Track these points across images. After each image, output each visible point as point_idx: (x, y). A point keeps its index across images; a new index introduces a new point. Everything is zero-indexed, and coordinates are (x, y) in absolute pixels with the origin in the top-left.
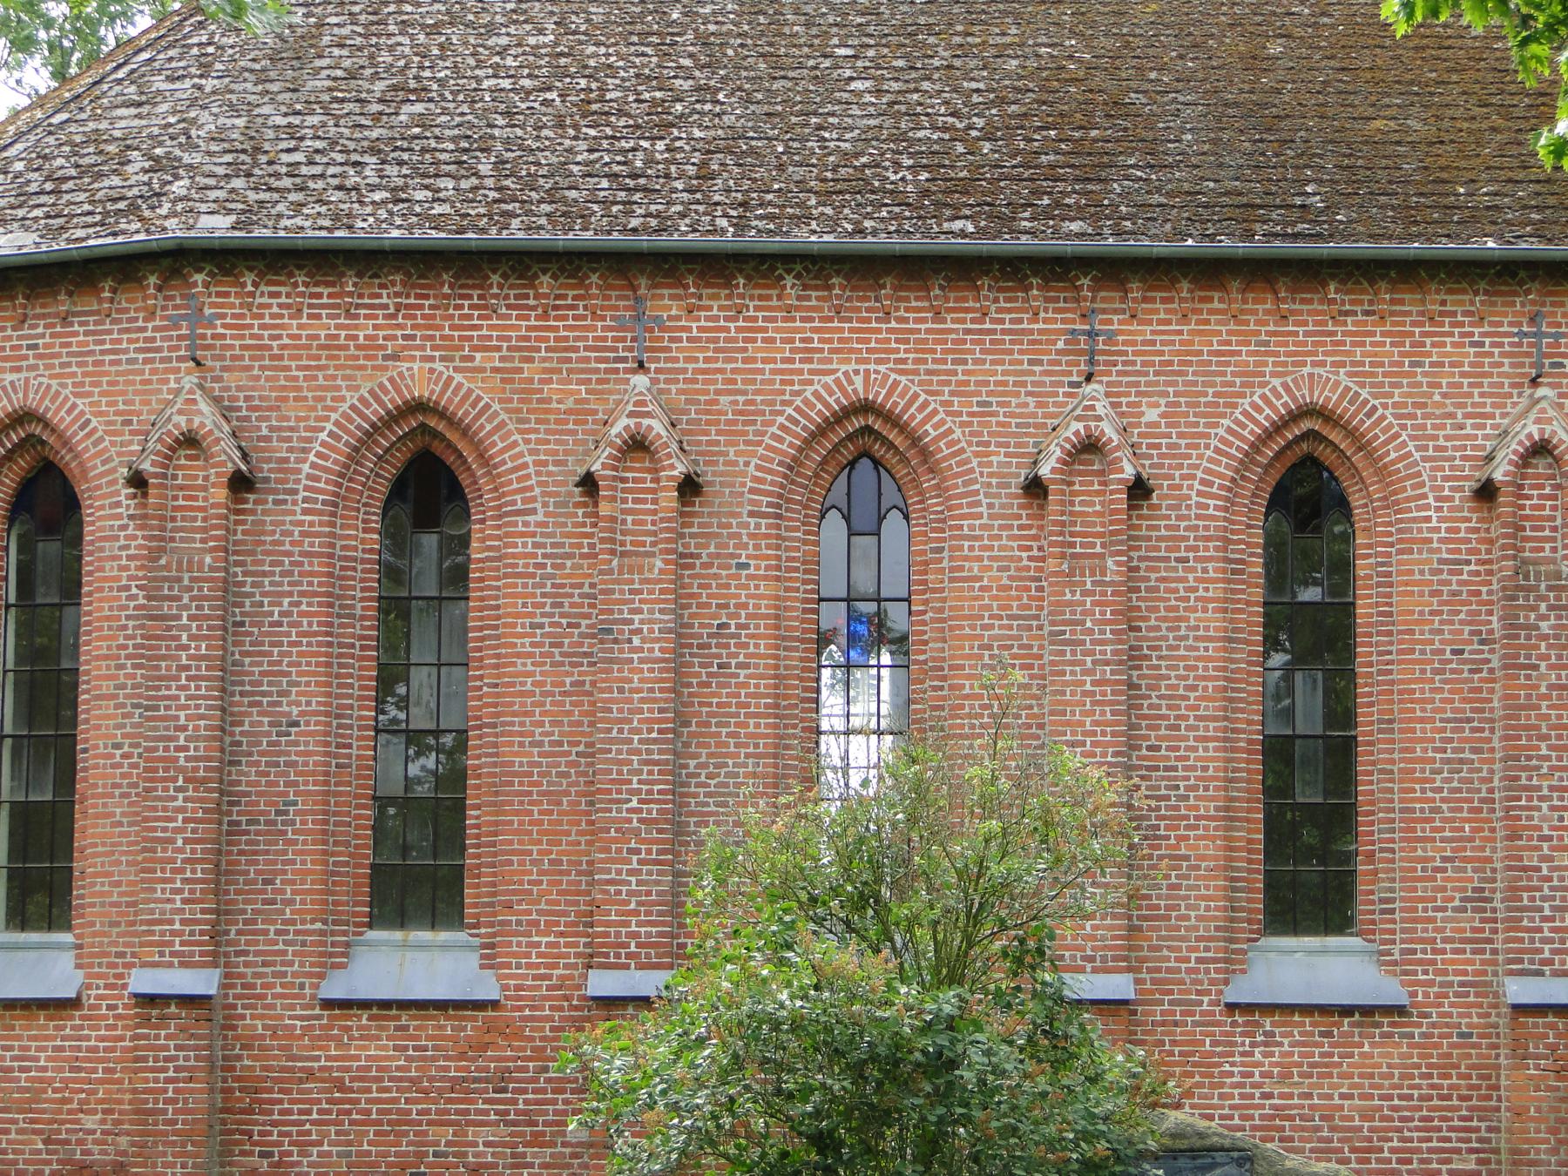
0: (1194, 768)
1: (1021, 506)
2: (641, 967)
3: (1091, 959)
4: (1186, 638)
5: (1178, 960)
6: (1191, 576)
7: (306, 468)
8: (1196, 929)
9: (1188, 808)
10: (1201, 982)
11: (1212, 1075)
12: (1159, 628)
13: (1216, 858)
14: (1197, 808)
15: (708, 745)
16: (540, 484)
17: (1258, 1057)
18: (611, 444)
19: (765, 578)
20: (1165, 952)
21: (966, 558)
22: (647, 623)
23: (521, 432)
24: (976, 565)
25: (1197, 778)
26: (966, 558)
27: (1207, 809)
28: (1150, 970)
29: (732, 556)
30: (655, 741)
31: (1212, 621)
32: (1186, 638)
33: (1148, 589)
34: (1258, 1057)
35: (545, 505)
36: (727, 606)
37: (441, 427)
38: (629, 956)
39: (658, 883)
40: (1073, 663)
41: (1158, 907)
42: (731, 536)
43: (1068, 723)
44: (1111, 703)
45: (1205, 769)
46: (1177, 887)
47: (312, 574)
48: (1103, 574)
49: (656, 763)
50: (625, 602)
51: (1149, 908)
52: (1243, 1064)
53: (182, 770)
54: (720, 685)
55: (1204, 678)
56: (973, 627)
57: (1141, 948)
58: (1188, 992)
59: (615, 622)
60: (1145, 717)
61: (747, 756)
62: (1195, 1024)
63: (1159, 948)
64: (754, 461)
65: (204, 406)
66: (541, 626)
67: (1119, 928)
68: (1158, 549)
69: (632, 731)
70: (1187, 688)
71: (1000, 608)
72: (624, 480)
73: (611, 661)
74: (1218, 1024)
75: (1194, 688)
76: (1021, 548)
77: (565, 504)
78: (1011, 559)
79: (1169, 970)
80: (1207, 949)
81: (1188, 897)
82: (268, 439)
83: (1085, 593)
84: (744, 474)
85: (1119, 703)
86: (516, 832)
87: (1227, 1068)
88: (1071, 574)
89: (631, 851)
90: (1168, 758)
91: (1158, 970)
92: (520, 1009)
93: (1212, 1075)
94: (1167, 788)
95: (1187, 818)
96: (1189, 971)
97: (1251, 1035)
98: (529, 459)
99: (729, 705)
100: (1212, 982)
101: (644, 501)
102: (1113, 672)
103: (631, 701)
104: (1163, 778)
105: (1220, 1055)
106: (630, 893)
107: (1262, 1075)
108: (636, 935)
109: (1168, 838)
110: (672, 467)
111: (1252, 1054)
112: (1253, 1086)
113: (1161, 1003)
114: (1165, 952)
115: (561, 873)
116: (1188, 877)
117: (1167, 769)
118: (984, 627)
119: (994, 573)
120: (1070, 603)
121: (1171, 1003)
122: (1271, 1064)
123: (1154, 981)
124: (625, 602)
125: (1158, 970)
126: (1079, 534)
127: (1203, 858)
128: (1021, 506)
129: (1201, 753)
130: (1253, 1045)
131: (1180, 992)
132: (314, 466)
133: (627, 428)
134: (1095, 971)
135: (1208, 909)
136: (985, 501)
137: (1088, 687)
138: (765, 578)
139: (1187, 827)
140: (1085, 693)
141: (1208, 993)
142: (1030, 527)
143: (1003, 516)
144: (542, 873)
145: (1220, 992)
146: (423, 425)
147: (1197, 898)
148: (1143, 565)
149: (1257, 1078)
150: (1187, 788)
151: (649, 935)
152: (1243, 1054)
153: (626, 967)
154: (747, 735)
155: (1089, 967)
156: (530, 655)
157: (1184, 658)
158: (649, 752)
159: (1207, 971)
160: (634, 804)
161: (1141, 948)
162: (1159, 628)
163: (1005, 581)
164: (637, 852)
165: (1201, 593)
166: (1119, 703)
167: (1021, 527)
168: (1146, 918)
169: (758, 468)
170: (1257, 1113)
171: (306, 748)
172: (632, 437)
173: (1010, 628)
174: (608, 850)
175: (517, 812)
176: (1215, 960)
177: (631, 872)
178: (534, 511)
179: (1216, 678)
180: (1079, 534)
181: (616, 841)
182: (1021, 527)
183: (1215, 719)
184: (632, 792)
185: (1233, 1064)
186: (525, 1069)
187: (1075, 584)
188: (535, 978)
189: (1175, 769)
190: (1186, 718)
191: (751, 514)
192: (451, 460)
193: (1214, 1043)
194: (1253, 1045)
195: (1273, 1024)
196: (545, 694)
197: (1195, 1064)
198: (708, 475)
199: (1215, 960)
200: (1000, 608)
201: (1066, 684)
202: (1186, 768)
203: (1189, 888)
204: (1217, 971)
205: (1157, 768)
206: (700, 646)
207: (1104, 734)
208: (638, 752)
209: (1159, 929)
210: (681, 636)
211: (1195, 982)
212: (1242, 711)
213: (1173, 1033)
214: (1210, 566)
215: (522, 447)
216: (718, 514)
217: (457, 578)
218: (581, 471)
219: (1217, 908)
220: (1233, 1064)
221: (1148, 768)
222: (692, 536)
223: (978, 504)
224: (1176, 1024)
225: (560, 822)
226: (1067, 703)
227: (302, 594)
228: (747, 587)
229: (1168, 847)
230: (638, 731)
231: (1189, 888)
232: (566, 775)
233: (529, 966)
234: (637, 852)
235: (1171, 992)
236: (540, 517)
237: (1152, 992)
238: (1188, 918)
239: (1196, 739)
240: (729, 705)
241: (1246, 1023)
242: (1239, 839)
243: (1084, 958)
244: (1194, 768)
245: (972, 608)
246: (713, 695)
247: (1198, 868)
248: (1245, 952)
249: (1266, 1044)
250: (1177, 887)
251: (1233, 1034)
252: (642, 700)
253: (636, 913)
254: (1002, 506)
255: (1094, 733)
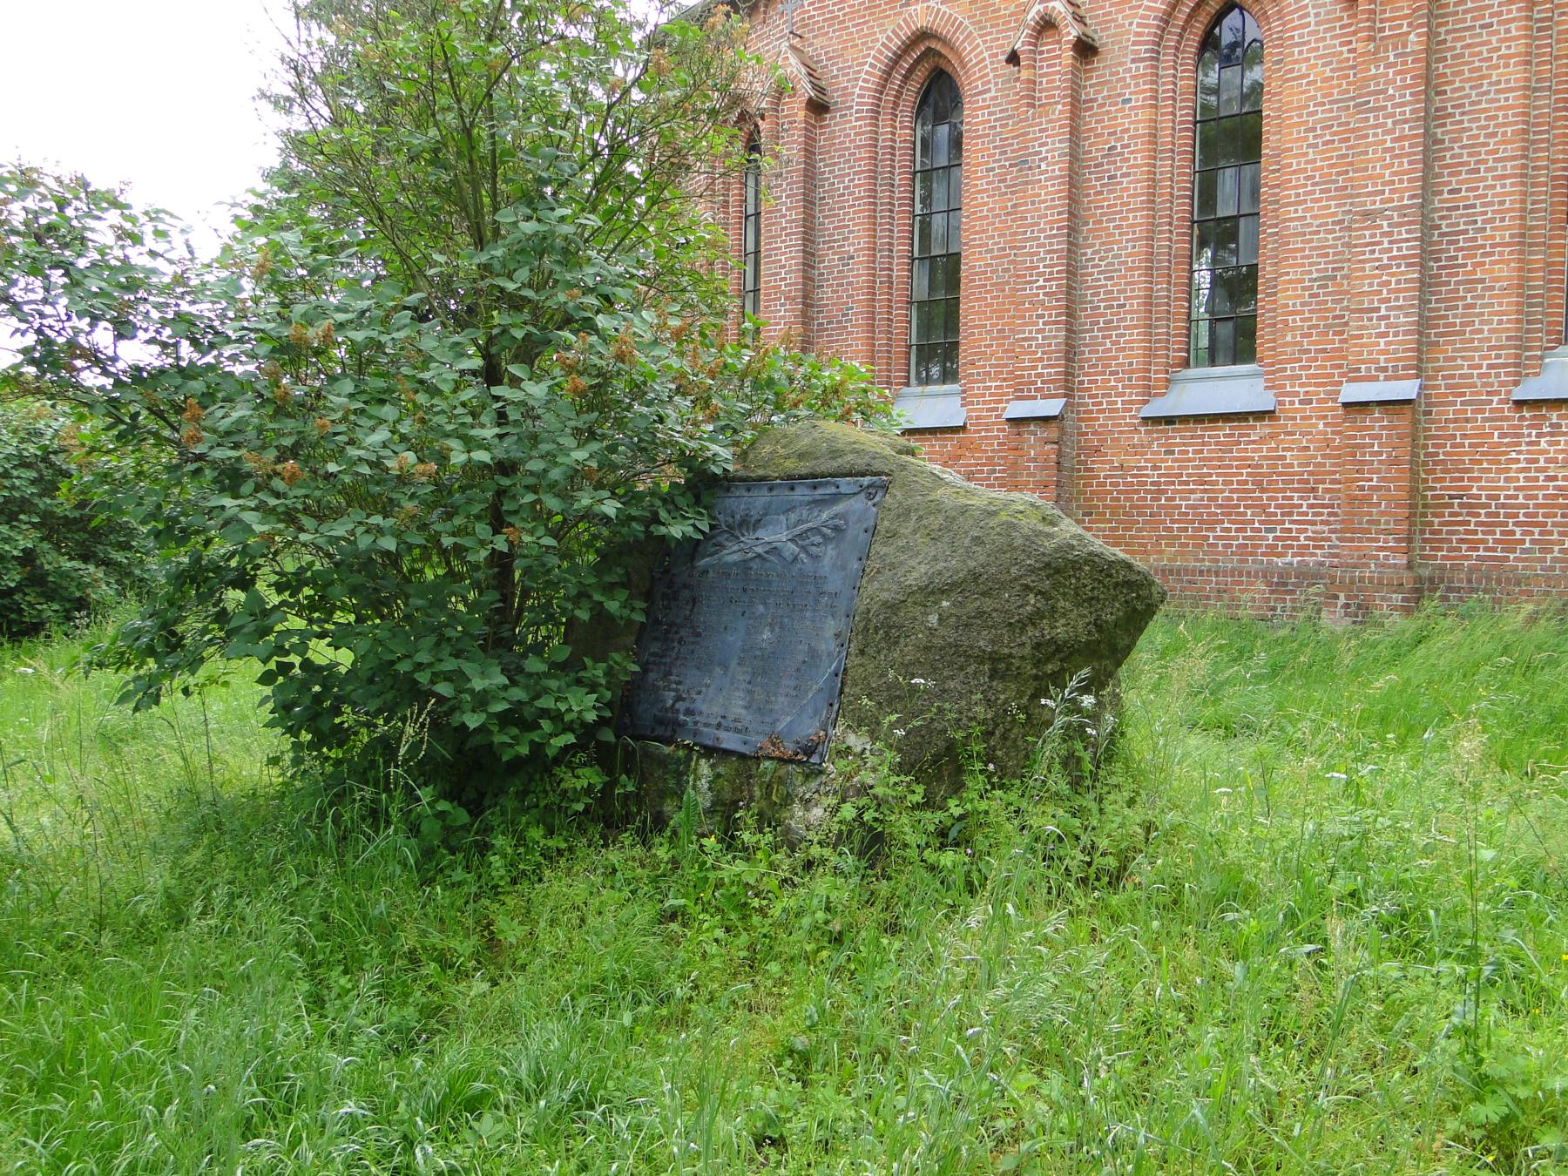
0: (1491, 204)
1: (1343, 10)
2: (1044, 397)
3: (1385, 369)
4: (1488, 92)
5: (1470, 367)
6: (1494, 39)
7: (857, 91)
8: (1489, 340)
9: (1485, 238)
10: (1492, 385)
11: (1499, 462)
12: (1463, 89)
13: (1509, 278)
14: (1493, 237)
15: (1100, 237)
16: (993, 70)
17: (1544, 445)
18: (1028, 26)
19: (1142, 107)
20: (1459, 362)
21: (1296, 62)
22: (1052, 150)
23: (981, 36)
24: (1304, 66)
25: (1494, 212)
26: (1296, 62)
27: (1503, 237)
28: (1444, 377)
29: (1120, 95)
30: (1055, 236)
31: (1514, 74)
32: (1488, 92)
33: (1454, 57)
34: (1544, 445)
35: (996, 84)
36: (1115, 133)
37: (938, 47)
38: (1037, 390)
39: (1055, 337)
40: (1376, 126)
41: (1454, 325)
42: (1118, 81)
43: (1370, 177)
44: (1409, 154)
45: (1502, 203)
46: (1473, 306)
47: (861, 159)
48: (1405, 46)
49: (1056, 251)
50: (1036, 139)
51: (1446, 325)
52: (1528, 452)
53: (783, 293)
54: (1110, 192)
55: (1505, 125)
56: (1300, 116)
57: (1438, 360)
58: (1479, 393)
59: (1030, 154)
60: (1447, 166)
61: (1128, 241)
62: (1485, 420)
63: (1454, 359)
64: (1137, 20)
65: (793, 60)
66: (993, 169)
67: (1410, 342)
68: (1464, 21)
69: (1040, 231)
70: (1488, 136)
71: (1324, 96)
72: (1041, 53)
73: (1027, 183)
74: (1507, 419)
75: (1494, 135)
76: (1342, 44)
77: (1008, 81)
78: (1333, 54)
79: (1462, 376)
80: (1498, 357)
81: (1482, 314)
82: (836, 77)
83: (1388, 66)
84: (1128, 32)
85: (1415, 154)
86: (977, 313)
87: (1514, 455)
88: (1377, 51)
89: (1039, 316)
90: (1467, 198)
91: (1453, 377)
92: (978, 431)
93: (1499, 462)
94: (1465, 223)
95: (1483, 247)
96: (1480, 376)
97: (1539, 427)
98: (986, 54)
99: (1115, 205)
100: (1502, 384)
101: (1054, 65)
102: (1411, 129)
103: (1038, 210)
104: (1462, 216)
105: (1507, 445)
106: (1038, 346)
107: (1547, 461)
108: (1040, 375)
109: (1465, 265)
110: (1069, 33)
111: (1538, 443)
112: (1538, 470)
113: (1454, 403)
114: (1459, 362)
115: (1004, 338)
116: (1483, 297)
117: (1465, 207)
118: (1310, 114)
119: (1320, 69)
120: (1375, 77)
121: (1463, 403)
122: (1556, 451)
123: (1448, 387)
124: (1036, 139)
125: (1453, 377)
126: (1388, 20)
127: (1498, 280)
128: (1343, 10)
129: (1498, 189)
130: (1539, 435)
131: (1472, 393)
132: (862, 88)
133: (1038, 12)
134: (1387, 379)
135: (1500, 322)
136: (1312, 12)
137: (1388, 144)
138: (1142, 107)
139: (1484, 255)
140: (1386, 150)
141: (1498, 393)
142: (1350, 25)
143: (1328, 21)
144: (992, 339)
145: (1509, 392)
146: (929, 49)
147: (1490, 314)
148: (1449, 38)
149: (1542, 463)
150: (1484, 221)
151: (1049, 374)
152: (1528, 444)
153: (1035, 398)
154: (1128, 226)
155: (1382, 376)
156: (986, 190)
157: (1485, 110)
158: (1051, 244)
159: (1498, 375)
160: (1041, 283)
161: (1438, 360)
162: (1463, 89)
163: (1328, 74)
164: (1042, 316)
165: (1503, 51)
166: (1415, 154)
167: (1342, 27)
168: (1442, 335)
169: (1139, 25)
170: (1541, 493)
171: (858, 273)
172: (1042, 18)
173: (1331, 111)
174: (1024, 317)
175: (977, 300)
176: (1504, 366)
177: (1038, 331)
178: (989, 90)
179: (1516, 123)
180: (1388, 20)
181: (1027, 310)
182: (1342, 27)
183: (1514, 158)
184: (1039, 274)
185: (1519, 452)
186: (982, 471)
187: (1379, 60)
188: (988, 410)
189: (1474, 206)
190: (1485, 161)
191: (1133, 61)
192: (950, 70)
193: (1501, 436)
194: (1539, 435)
195: (1559, 417)
196: (995, 216)
197: (1483, 454)
198: (1101, 38)
199: (1504, 366)
200: (1324, 96)
201: (1369, 145)
202: (1484, 205)
203: (1483, 306)
204: (1507, 374)
205: (1457, 208)
206: (1096, 166)
207: (1401, 181)
208: (1044, 245)
209: (1454, 342)
210: (1075, 156)
211: (1485, 385)
212: (1542, 150)
213: (1465, 429)
214: (1513, 26)
215: (982, 47)
216: (1110, 66)
217: (956, 143)
218: (1009, 49)
219: (1509, 321)
220: (1519, 452)
221: (1448, 209)
222: (1091, 86)
223: (1307, 15)
224: (1467, 420)
225: (1003, 304)
226: (1369, 161)
227: (855, 173)
228: (1129, 116)
229: (1465, 273)
230: (1044, 231)
231: (1483, 306)
232: (1008, 270)
233: (984, 402)
234: (1042, 316)
235: (1464, 394)
236: (993, 94)
237: (1446, 395)
238: (1482, 331)
239: (1494, 178)
240: (1115, 205)
241: (1534, 417)
242: (1536, 261)
243: (1377, 369)
244: (1491, 204)
245: (1299, 100)
246: (1105, 199)
247: (1493, 288)
248: (1541, 358)
249: (1551, 434)
250: (1473, 306)
251: (1521, 427)
252: (1047, 208)
253: (1041, 360)
254: (1327, 13)
255: (1393, 182)
